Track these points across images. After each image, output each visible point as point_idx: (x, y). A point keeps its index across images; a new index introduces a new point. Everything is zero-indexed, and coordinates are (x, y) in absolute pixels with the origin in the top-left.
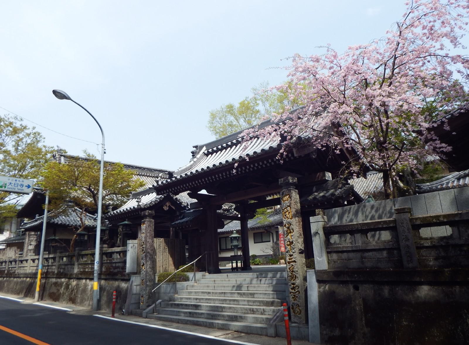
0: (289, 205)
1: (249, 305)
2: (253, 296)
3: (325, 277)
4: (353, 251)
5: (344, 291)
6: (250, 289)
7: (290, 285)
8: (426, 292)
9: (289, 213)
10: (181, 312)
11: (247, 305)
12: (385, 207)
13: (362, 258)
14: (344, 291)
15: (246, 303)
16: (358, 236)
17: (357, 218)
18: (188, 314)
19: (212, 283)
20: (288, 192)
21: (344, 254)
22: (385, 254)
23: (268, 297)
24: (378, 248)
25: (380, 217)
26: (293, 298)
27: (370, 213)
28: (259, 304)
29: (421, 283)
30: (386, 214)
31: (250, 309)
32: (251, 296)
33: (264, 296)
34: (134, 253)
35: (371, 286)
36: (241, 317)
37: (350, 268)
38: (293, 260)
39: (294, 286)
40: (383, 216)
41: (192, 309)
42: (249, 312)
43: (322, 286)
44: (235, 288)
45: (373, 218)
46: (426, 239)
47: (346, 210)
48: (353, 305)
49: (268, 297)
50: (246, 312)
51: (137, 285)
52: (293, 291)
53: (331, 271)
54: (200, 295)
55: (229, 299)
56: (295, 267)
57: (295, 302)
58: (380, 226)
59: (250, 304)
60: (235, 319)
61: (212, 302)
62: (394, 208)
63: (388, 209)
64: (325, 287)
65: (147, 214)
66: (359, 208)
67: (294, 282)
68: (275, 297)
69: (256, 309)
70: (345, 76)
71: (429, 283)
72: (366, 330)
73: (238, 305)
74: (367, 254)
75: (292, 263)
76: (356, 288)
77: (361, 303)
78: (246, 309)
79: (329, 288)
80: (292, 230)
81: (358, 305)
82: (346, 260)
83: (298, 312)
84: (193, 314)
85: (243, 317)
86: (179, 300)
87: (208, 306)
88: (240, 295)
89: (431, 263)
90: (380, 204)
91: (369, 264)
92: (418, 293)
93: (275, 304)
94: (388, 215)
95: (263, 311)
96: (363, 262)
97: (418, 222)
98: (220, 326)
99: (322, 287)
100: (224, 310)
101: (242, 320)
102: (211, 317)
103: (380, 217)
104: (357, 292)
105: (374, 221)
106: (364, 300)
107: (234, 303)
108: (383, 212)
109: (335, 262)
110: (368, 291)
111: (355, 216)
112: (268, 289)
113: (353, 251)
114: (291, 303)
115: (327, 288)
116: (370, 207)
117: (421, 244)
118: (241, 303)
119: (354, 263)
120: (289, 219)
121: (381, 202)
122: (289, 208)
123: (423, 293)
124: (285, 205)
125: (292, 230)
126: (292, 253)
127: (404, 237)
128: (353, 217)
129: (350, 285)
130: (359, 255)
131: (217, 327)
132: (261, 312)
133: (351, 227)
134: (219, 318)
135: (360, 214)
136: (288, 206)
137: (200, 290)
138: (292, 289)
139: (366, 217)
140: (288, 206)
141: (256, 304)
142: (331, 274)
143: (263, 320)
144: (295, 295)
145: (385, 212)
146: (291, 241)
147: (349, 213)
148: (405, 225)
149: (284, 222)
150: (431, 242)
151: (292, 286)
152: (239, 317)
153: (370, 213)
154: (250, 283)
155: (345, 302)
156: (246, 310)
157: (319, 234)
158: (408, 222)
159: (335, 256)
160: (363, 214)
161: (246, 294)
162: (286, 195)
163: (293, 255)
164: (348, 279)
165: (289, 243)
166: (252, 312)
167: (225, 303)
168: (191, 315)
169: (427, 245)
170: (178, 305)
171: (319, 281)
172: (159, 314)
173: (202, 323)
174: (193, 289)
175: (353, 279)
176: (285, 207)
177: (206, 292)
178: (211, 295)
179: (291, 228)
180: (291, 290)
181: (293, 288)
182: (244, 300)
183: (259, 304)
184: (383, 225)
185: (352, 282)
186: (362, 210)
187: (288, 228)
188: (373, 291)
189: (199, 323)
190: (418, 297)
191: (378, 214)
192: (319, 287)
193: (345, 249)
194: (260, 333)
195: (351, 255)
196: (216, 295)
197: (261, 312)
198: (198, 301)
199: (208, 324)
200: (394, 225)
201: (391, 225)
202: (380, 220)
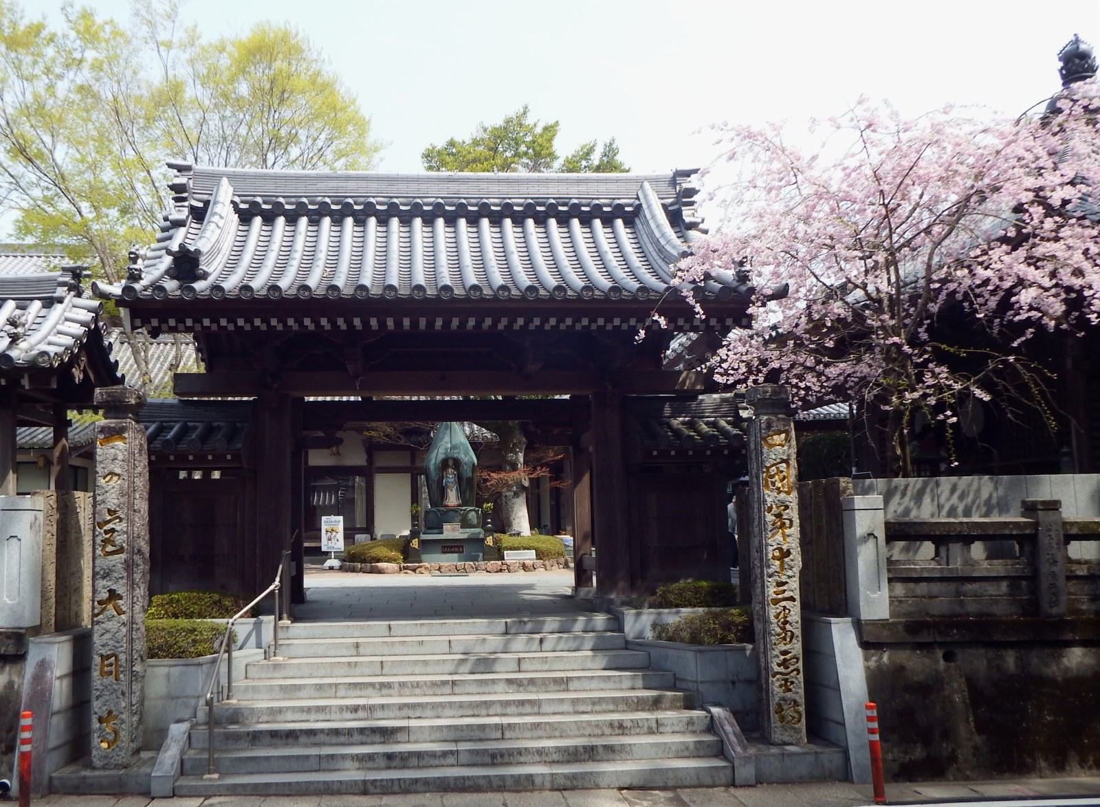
0: (785, 458)
1: (577, 713)
2: (563, 687)
3: (885, 636)
4: (942, 579)
5: (916, 663)
6: (524, 666)
7: (777, 656)
8: (1079, 659)
9: (784, 478)
10: (344, 757)
11: (568, 713)
12: (978, 491)
13: (958, 594)
14: (916, 663)
15: (567, 707)
16: (956, 548)
17: (919, 507)
18: (382, 762)
19: (345, 652)
20: (784, 426)
21: (921, 584)
22: (1004, 586)
23: (618, 686)
24: (994, 575)
25: (967, 513)
26: (781, 686)
27: (948, 500)
28: (611, 707)
29: (1070, 644)
30: (978, 507)
31: (611, 725)
32: (557, 688)
33: (602, 685)
34: (36, 548)
35: (982, 651)
36: (610, 749)
37: (934, 616)
38: (787, 594)
39: (788, 657)
40: (974, 509)
41: (362, 744)
42: (608, 731)
43: (873, 656)
44: (467, 667)
45: (952, 512)
46: (1078, 562)
47: (896, 487)
48: (947, 692)
49: (618, 686)
50: (599, 732)
51: (60, 678)
52: (781, 669)
53: (900, 623)
54: (340, 694)
55: (500, 702)
56: (792, 613)
57: (789, 695)
58: (1007, 532)
59: (582, 708)
60: (587, 756)
61: (429, 713)
62: (995, 495)
63: (985, 495)
64: (881, 658)
65: (133, 402)
66: (925, 485)
67: (788, 646)
68: (640, 683)
69: (632, 721)
70: (1060, 212)
71: (1084, 644)
72: (978, 739)
73: (539, 714)
74: (969, 587)
75: (784, 603)
76: (948, 657)
77: (964, 687)
78: (597, 725)
79: (889, 659)
80: (787, 522)
81: (957, 693)
82: (924, 597)
83: (794, 718)
84: (502, 756)
85: (616, 748)
86: (265, 718)
87: (440, 728)
88: (515, 686)
89: (1084, 607)
90: (970, 485)
91: (972, 607)
92: (1065, 661)
93: (666, 703)
94: (984, 510)
95: (654, 725)
96: (961, 603)
97: (1074, 531)
98: (562, 781)
99: (874, 658)
100: (508, 734)
101: (611, 756)
102: (488, 760)
103: (967, 513)
104: (953, 664)
105: (952, 520)
106: (971, 682)
107: (521, 709)
108: (973, 502)
109: (900, 602)
110: (976, 662)
111: (915, 503)
112: (589, 665)
113: (942, 579)
114: (777, 699)
115: (885, 658)
116: (950, 487)
117: (1072, 571)
118: (545, 708)
119: (942, 605)
120: (782, 495)
121: (972, 480)
122: (784, 465)
123: (1075, 661)
124: (774, 457)
125: (787, 522)
126: (784, 579)
127: (1050, 556)
128: (912, 503)
129: (938, 651)
130: (952, 587)
131: (548, 785)
132: (650, 728)
133: (947, 529)
134: (522, 759)
135: (927, 499)
136: (783, 461)
137: (311, 677)
138: (779, 665)
139: (940, 507)
140: (783, 461)
141: (604, 707)
142: (900, 628)
143: (687, 748)
144: (786, 680)
145: (977, 502)
146: (785, 547)
147: (904, 494)
148: (1053, 534)
149: (769, 500)
150: (1089, 569)
151: (782, 657)
152: (601, 750)
153: (948, 500)
154: (501, 648)
155: (929, 688)
156: (597, 726)
157: (876, 537)
158: (1060, 529)
159: (900, 589)
160: (933, 500)
161: (525, 683)
162: (779, 433)
163: (787, 583)
164: (938, 639)
165: (777, 554)
166: (617, 731)
167: (484, 712)
168: (396, 763)
169: (1082, 574)
170: (255, 738)
171: (865, 645)
172: (223, 775)
173: (482, 782)
174: (277, 675)
175: (949, 639)
176: (773, 462)
177: (372, 685)
178: (395, 691)
179: (785, 517)
180: (777, 669)
181: (784, 663)
182: (562, 701)
183: (611, 707)
184: (1011, 529)
185: (941, 645)
186: (932, 490)
187: (779, 516)
188: (985, 662)
189: (467, 783)
190: (1067, 668)
191: (964, 504)
192: (867, 659)
193: (926, 575)
194: (709, 781)
195: (936, 588)
196: (418, 691)
197: (650, 728)
198: (361, 714)
199: (509, 782)
200: (1033, 532)
201: (1028, 532)
202: (965, 520)
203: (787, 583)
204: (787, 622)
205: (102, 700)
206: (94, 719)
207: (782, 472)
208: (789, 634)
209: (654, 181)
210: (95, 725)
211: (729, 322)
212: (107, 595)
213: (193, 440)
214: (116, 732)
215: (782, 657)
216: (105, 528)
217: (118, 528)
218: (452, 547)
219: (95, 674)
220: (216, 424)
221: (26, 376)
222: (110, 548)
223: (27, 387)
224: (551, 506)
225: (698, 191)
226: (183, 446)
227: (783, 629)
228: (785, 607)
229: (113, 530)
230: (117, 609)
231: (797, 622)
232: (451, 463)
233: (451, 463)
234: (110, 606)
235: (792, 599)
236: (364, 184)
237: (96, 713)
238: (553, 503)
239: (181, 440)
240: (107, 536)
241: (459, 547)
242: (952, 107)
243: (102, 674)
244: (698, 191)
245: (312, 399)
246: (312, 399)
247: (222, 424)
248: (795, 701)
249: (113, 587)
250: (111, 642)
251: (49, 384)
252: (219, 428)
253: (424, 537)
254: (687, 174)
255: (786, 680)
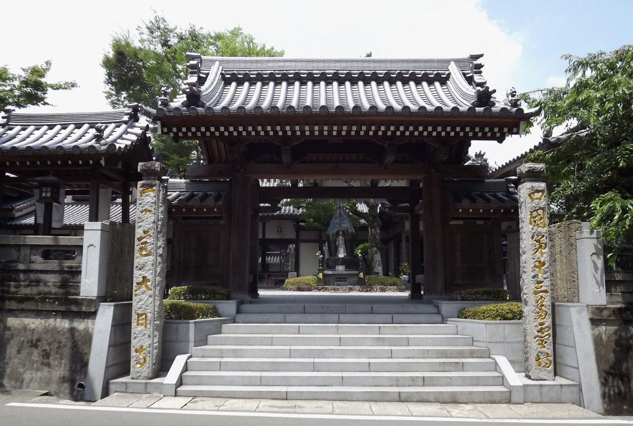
38: (543, 289)
80: (543, 245)
83: (547, 364)
125: (543, 245)
140: (540, 208)
151: (540, 327)
163: (543, 281)
203: (543, 281)
204: (543, 305)
205: (137, 339)
206: (133, 349)
207: (540, 215)
208: (545, 312)
209: (457, 61)
210: (133, 354)
211: (506, 130)
212: (142, 279)
213: (196, 199)
214: (145, 359)
215: (540, 327)
216: (142, 241)
217: (148, 241)
218: (340, 278)
219: (134, 324)
220: (209, 193)
221: (103, 158)
222: (144, 253)
223: (103, 165)
224: (395, 261)
225: (483, 66)
226: (190, 203)
227: (541, 309)
228: (542, 296)
229: (146, 243)
230: (147, 287)
231: (549, 306)
232: (341, 233)
233: (341, 233)
234: (143, 286)
235: (546, 291)
236: (293, 64)
237: (134, 347)
238: (396, 259)
239: (190, 200)
240: (143, 246)
241: (344, 278)
242: (617, 51)
243: (138, 324)
244: (483, 66)
245: (267, 205)
246: (267, 205)
247: (212, 193)
248: (548, 354)
249: (146, 275)
250: (143, 306)
251: (117, 165)
252: (211, 195)
253: (326, 272)
254: (477, 57)
255: (542, 341)
